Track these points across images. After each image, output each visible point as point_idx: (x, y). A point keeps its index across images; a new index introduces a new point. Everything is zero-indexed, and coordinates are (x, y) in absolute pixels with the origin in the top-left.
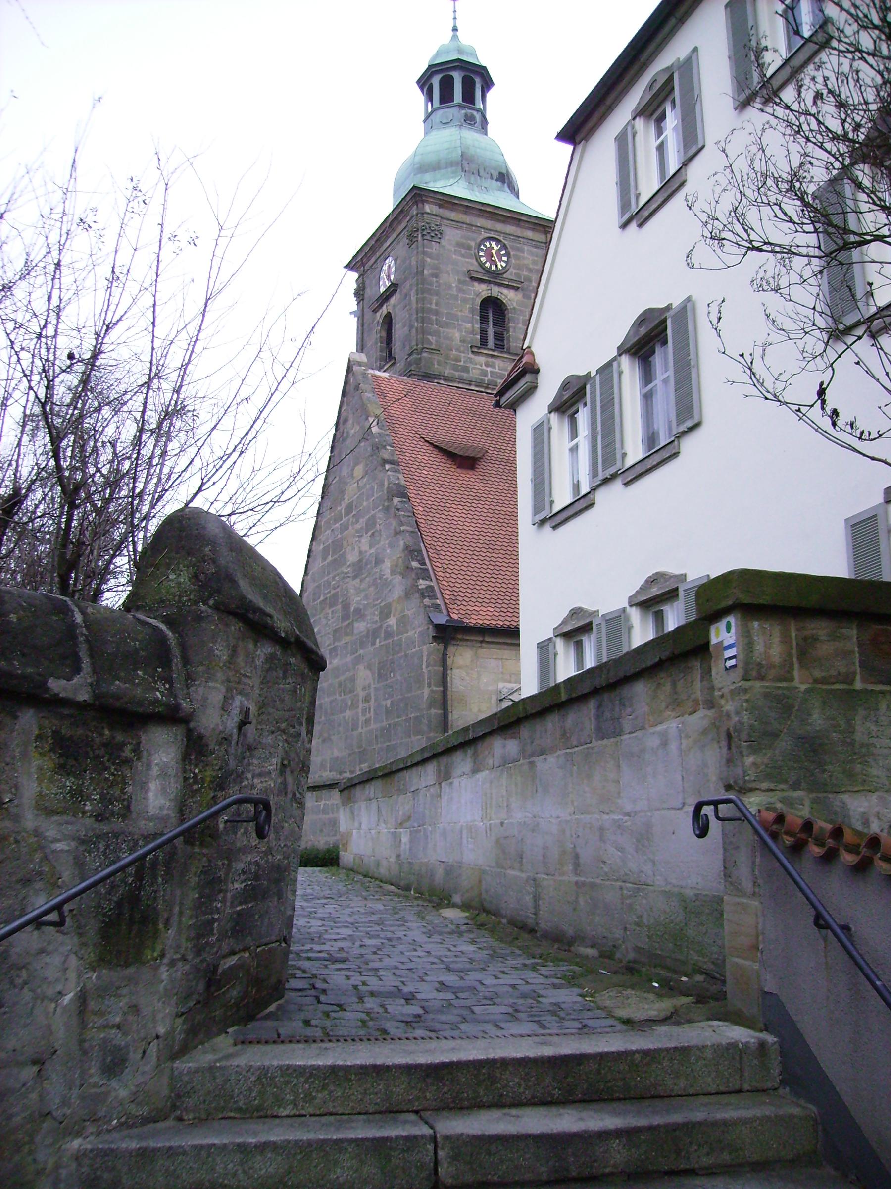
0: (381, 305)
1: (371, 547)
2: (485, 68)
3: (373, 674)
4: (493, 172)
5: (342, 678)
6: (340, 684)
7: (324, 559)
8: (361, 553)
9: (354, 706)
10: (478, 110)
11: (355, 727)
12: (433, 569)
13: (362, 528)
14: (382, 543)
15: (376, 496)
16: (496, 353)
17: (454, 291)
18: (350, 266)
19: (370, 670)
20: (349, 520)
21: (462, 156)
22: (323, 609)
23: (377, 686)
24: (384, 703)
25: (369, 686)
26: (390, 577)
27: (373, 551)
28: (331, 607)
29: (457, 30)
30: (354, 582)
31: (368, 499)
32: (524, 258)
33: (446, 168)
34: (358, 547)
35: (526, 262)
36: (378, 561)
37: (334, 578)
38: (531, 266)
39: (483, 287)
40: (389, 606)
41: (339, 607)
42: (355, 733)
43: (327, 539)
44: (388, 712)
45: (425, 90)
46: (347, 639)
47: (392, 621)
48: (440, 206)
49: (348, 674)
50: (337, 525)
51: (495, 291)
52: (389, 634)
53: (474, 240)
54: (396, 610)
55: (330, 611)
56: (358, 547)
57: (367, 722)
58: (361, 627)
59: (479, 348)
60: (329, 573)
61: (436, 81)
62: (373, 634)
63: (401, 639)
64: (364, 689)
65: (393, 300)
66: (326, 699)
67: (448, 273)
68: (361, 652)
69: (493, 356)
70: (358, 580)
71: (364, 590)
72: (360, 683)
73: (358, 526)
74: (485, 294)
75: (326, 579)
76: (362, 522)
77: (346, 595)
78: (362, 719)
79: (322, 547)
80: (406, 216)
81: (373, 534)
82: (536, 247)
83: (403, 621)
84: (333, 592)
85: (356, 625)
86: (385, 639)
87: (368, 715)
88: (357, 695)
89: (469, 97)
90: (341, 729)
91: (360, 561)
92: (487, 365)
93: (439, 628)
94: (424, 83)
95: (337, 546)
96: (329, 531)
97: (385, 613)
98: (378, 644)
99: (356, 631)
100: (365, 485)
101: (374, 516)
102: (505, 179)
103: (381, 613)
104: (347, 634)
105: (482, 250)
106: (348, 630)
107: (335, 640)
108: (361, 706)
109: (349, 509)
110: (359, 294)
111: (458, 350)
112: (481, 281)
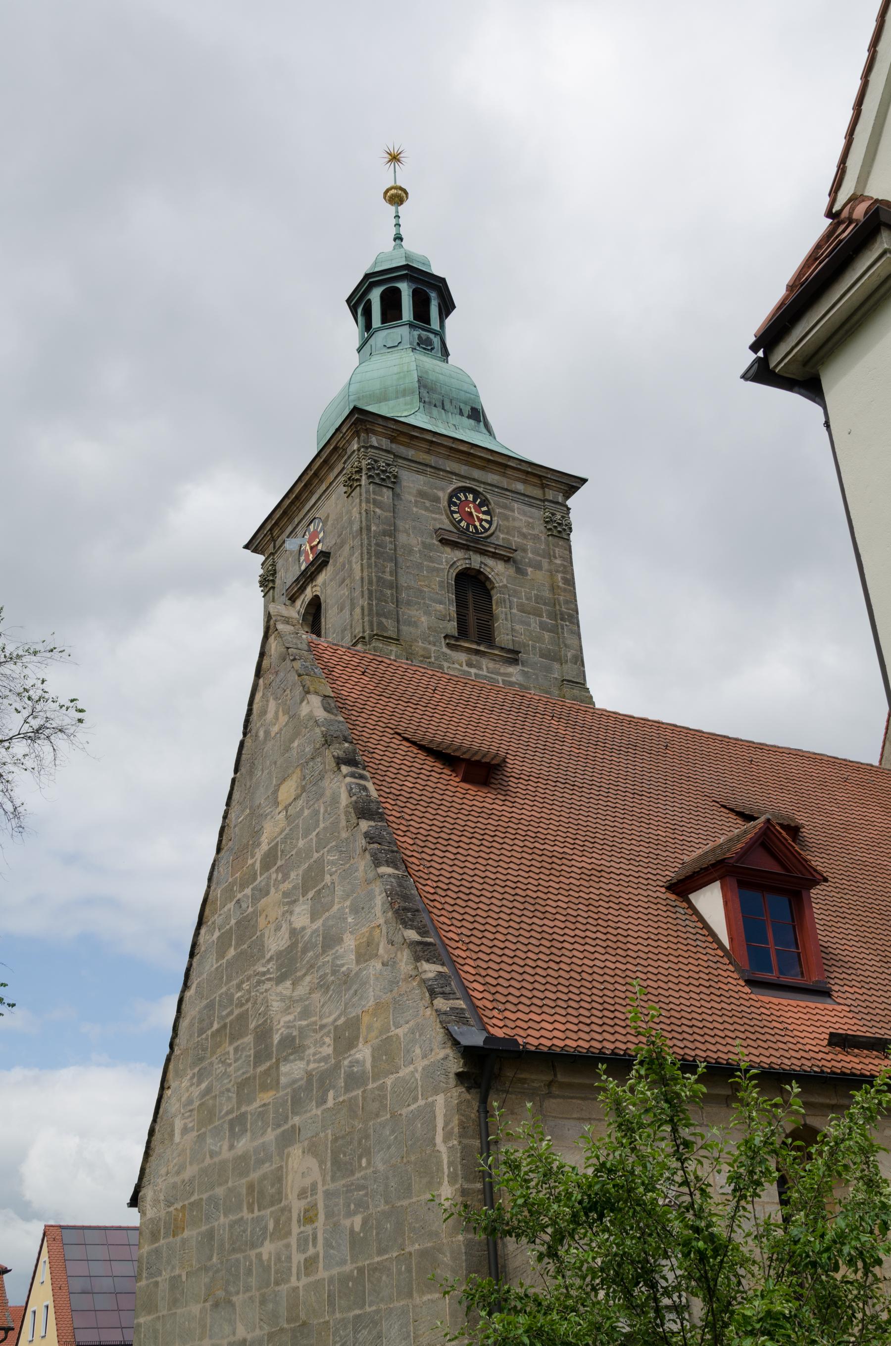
0: (302, 589)
1: (313, 919)
2: (443, 281)
3: (321, 1163)
4: (462, 406)
5: (255, 1176)
6: (251, 1187)
7: (221, 955)
8: (293, 932)
9: (281, 1232)
10: (435, 333)
11: (283, 1277)
12: (445, 945)
13: (295, 888)
14: (336, 907)
15: (322, 825)
16: (482, 648)
17: (416, 558)
18: (253, 545)
19: (315, 1155)
20: (269, 878)
21: (419, 380)
22: (218, 1045)
23: (331, 1186)
24: (347, 1223)
25: (314, 1186)
26: (355, 968)
27: (319, 923)
28: (233, 1038)
29: (401, 239)
30: (280, 988)
31: (306, 834)
32: (514, 519)
33: (397, 398)
34: (285, 920)
35: (517, 524)
36: (330, 940)
37: (239, 987)
38: (524, 530)
39: (459, 554)
40: (354, 1024)
41: (249, 1039)
42: (284, 1288)
43: (228, 917)
44: (357, 1243)
45: (360, 311)
46: (267, 1097)
47: (363, 1053)
48: (393, 440)
49: (266, 1168)
50: (248, 891)
51: (476, 561)
52: (354, 1080)
53: (443, 489)
54: (370, 1028)
55: (231, 1049)
56: (285, 920)
57: (310, 1264)
58: (293, 1070)
59: (457, 639)
60: (230, 979)
61: (375, 296)
62: (318, 1084)
63: (382, 1088)
64: (302, 1194)
65: (321, 578)
66: (222, 1219)
67: (406, 532)
68: (296, 1120)
69: (477, 652)
70: (288, 983)
71: (301, 1000)
72: (293, 1183)
73: (287, 886)
74: (461, 565)
75: (224, 989)
76: (296, 876)
77: (265, 1013)
78: (298, 1258)
79: (217, 934)
80: (341, 456)
81: (319, 892)
82: (531, 506)
83: (388, 1053)
84: (237, 1012)
85: (284, 1069)
86: (347, 1089)
87: (311, 1251)
88: (288, 1209)
89: (421, 315)
90: (253, 1281)
91: (293, 946)
92: (470, 665)
93: (469, 1053)
94: (357, 302)
95: (246, 927)
96: (231, 905)
97: (346, 1037)
98: (330, 1103)
99: (283, 1080)
100: (302, 810)
101: (320, 863)
102: (477, 415)
103: (336, 1039)
104: (264, 1088)
105: (455, 504)
106: (269, 1080)
107: (239, 1103)
108: (295, 1229)
109: (269, 861)
110: (267, 582)
111: (425, 640)
112: (454, 545)
